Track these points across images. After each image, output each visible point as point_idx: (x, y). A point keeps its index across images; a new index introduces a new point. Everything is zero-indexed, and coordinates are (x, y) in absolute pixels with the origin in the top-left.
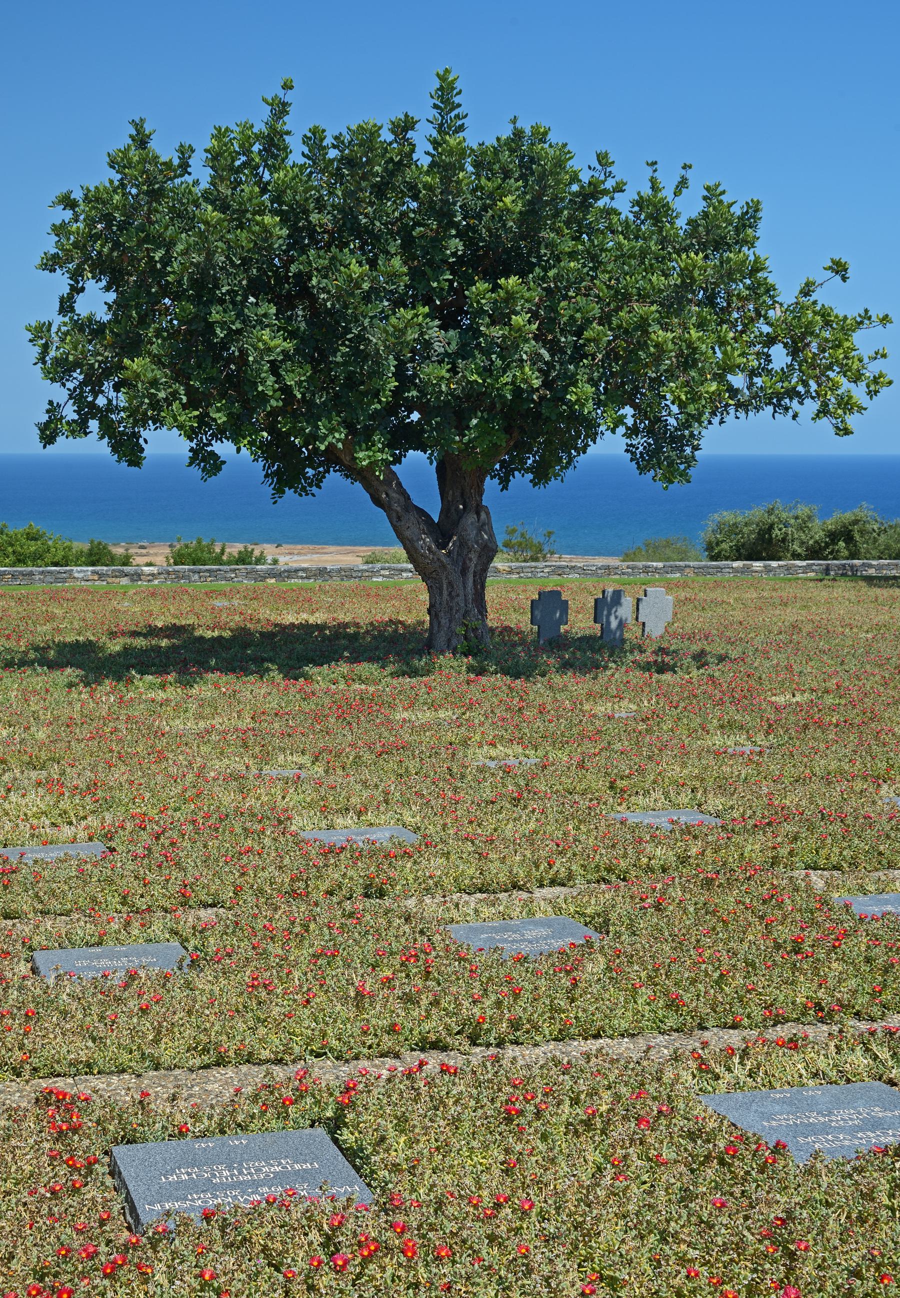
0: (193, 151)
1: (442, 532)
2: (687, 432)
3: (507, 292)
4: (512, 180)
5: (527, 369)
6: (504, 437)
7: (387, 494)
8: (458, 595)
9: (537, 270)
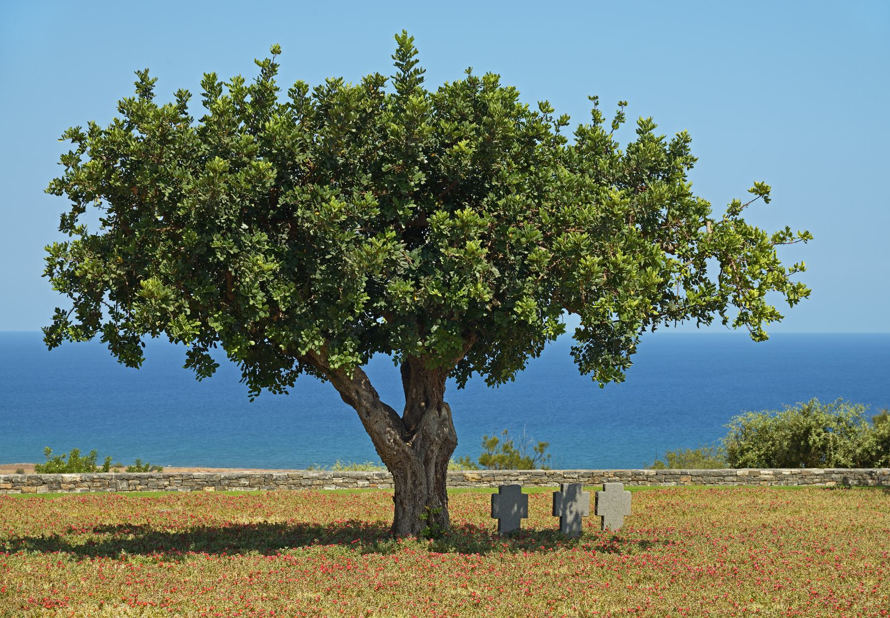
0: (190, 96)
1: (407, 426)
2: (623, 339)
3: (462, 221)
4: (467, 122)
5: (479, 286)
6: (461, 341)
7: (357, 392)
8: (421, 484)
9: (491, 195)
